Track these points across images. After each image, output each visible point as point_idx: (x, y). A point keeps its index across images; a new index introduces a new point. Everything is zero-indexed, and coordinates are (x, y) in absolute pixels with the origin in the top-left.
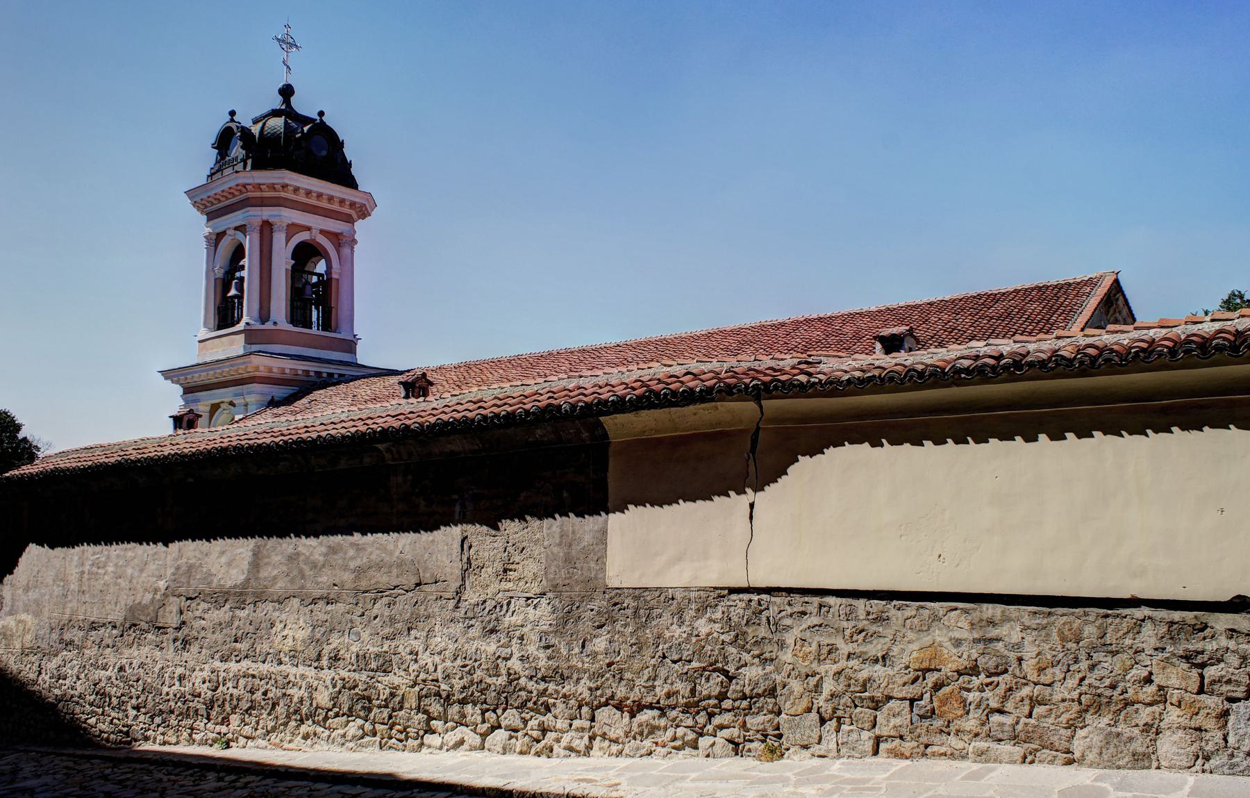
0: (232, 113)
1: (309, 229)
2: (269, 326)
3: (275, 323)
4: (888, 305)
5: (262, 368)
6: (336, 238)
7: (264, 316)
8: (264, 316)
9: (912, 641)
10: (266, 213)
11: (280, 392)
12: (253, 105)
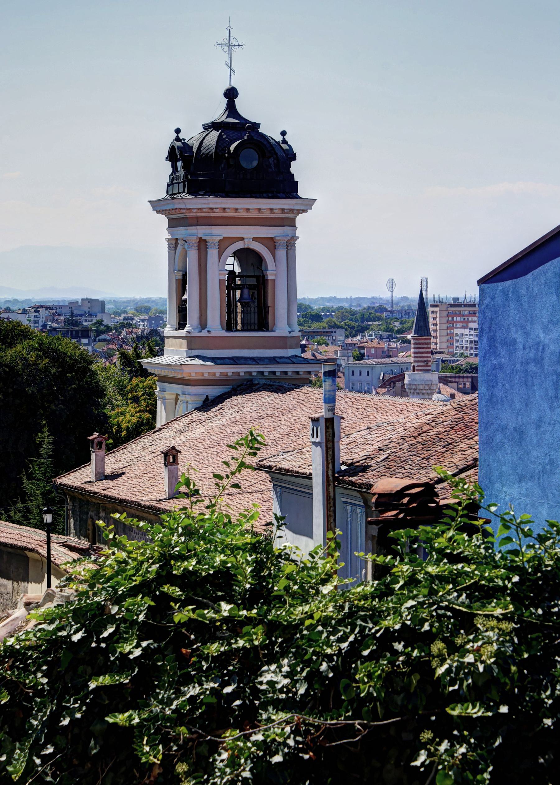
0: (178, 131)
1: (242, 239)
2: (204, 333)
3: (209, 332)
4: (381, 297)
5: (193, 375)
6: (271, 244)
7: (203, 325)
8: (203, 325)
9: (330, 430)
10: (201, 231)
11: (213, 391)
12: (195, 119)
